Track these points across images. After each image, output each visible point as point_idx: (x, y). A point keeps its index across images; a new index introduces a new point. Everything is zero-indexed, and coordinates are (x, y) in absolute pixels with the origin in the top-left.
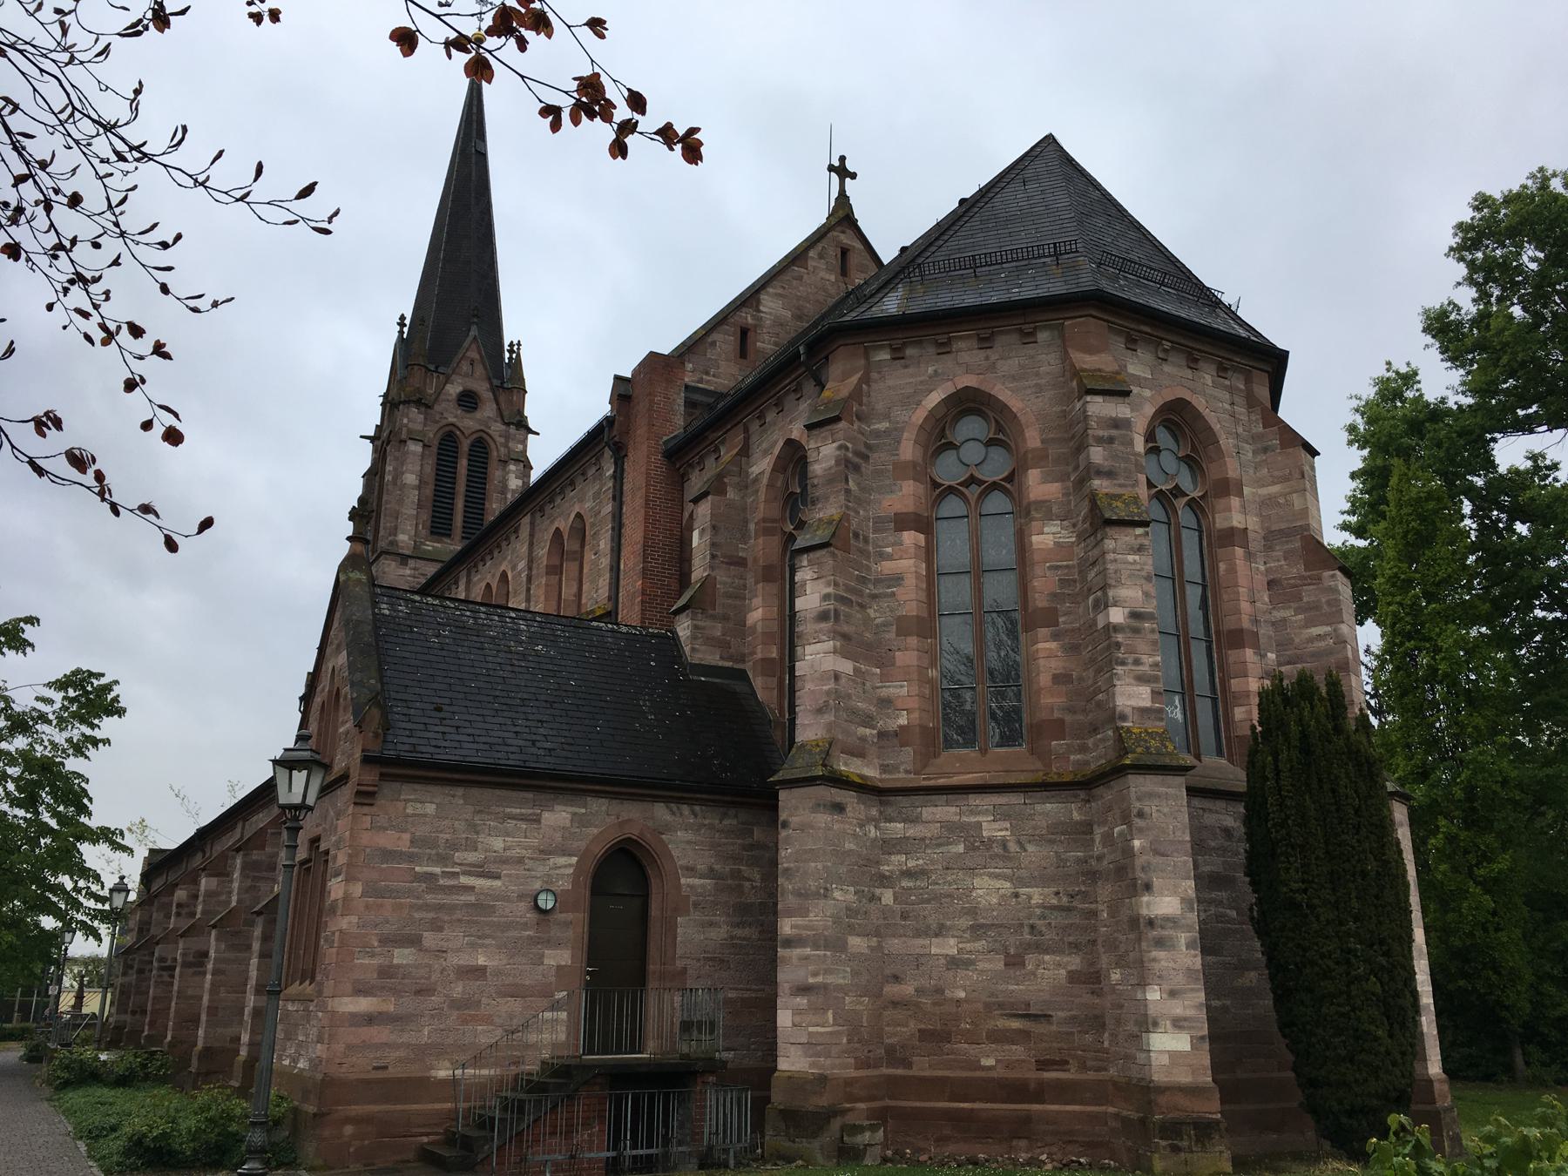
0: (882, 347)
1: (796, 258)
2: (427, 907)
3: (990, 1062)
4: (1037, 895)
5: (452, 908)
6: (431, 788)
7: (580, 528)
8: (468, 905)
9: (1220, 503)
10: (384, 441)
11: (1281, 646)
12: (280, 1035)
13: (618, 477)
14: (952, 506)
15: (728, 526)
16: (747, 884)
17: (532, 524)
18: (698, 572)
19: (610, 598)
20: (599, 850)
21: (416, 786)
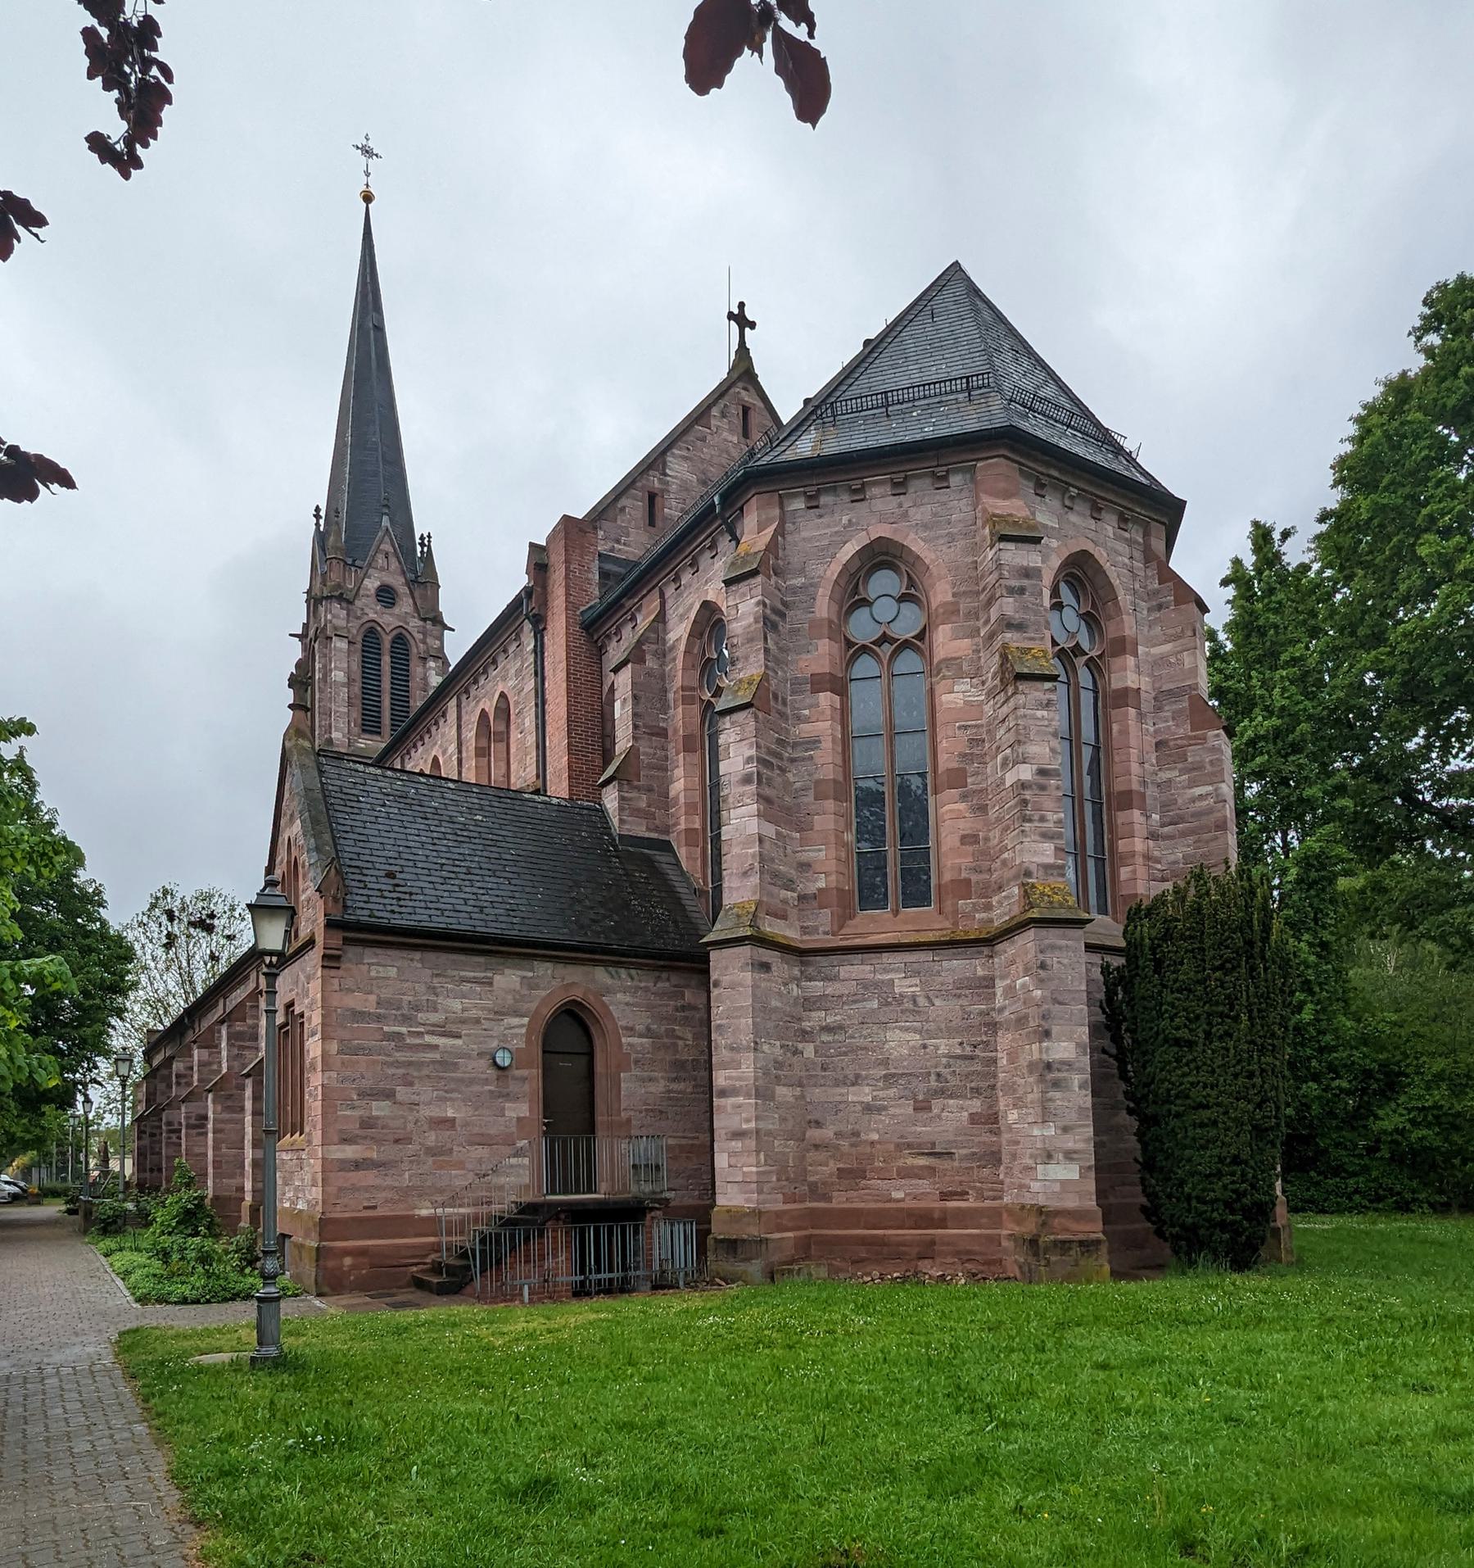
0: (795, 495)
1: (700, 416)
2: (397, 1064)
3: (900, 1195)
4: (944, 1046)
5: (420, 1065)
6: (390, 952)
7: (504, 708)
8: (433, 1062)
9: (1116, 663)
10: (312, 637)
11: (1165, 807)
12: (279, 1182)
13: (539, 651)
14: (865, 666)
15: (650, 696)
16: (681, 1043)
17: (459, 706)
18: (623, 740)
19: (538, 776)
20: (547, 1012)
21: (379, 951)
